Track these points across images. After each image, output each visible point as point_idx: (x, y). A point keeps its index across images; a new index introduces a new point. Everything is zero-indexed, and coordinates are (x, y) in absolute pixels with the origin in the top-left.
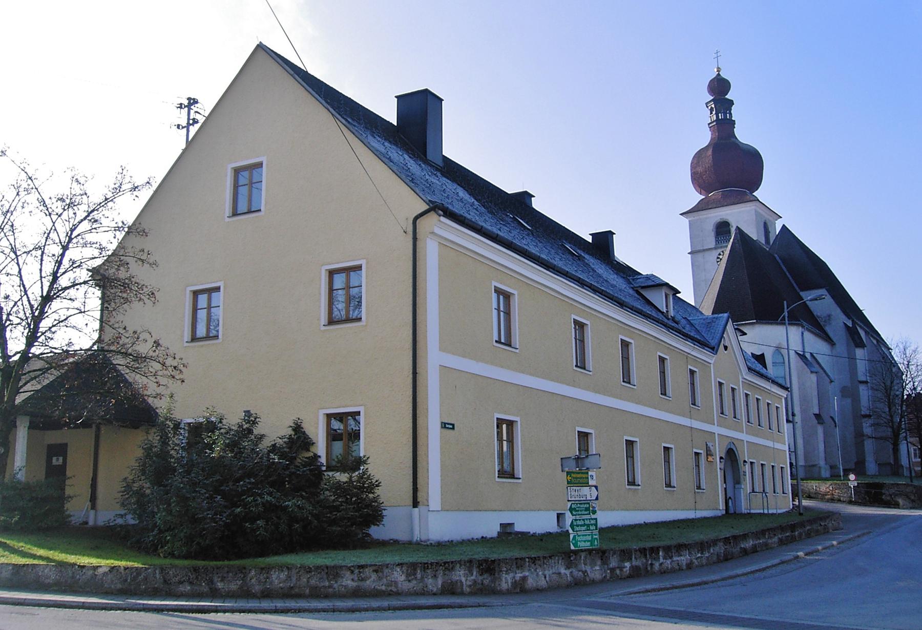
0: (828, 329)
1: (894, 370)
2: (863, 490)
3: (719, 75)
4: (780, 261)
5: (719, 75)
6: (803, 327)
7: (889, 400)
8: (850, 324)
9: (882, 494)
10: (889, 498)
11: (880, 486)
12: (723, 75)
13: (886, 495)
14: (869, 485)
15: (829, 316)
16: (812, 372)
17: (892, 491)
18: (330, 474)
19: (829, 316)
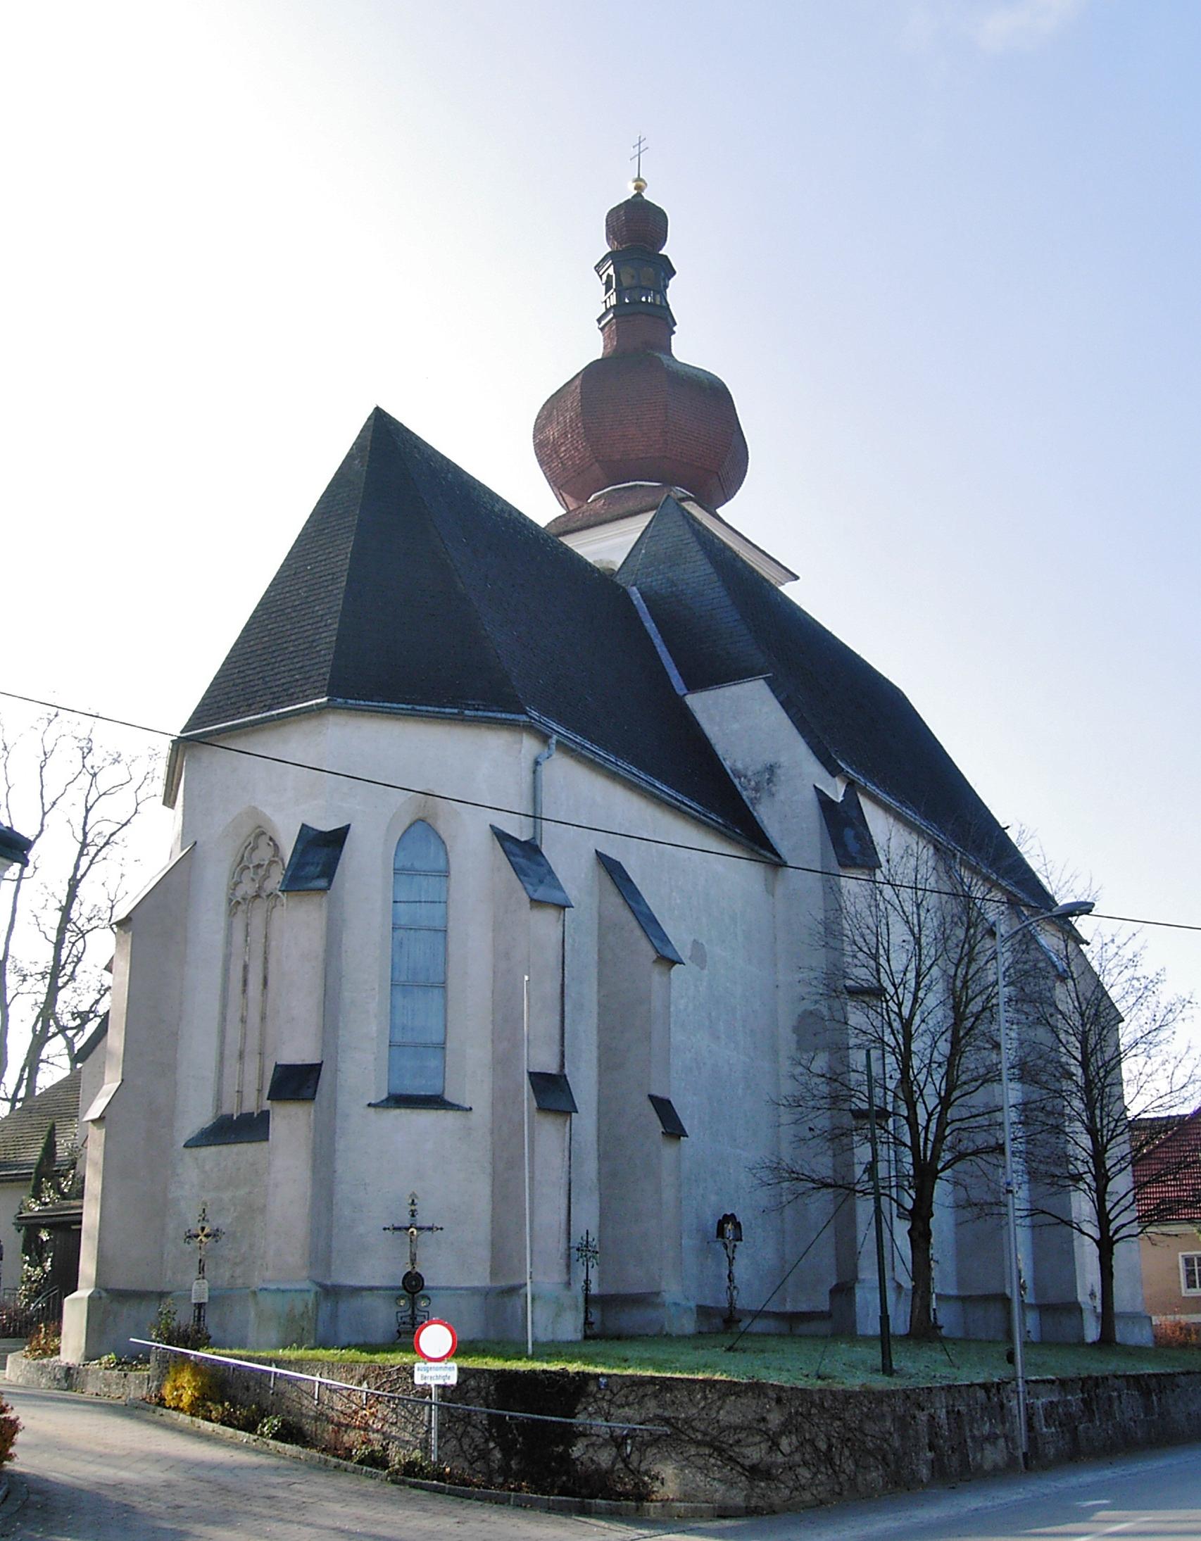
0: (767, 816)
1: (1063, 996)
2: (480, 1411)
3: (639, 195)
4: (650, 625)
5: (639, 195)
6: (544, 738)
7: (959, 1018)
8: (836, 791)
9: (570, 1435)
10: (605, 1458)
11: (569, 1391)
12: (647, 195)
13: (594, 1438)
14: (510, 1387)
15: (771, 769)
16: (536, 903)
17: (627, 1418)
18: (904, 1122)
19: (771, 769)
